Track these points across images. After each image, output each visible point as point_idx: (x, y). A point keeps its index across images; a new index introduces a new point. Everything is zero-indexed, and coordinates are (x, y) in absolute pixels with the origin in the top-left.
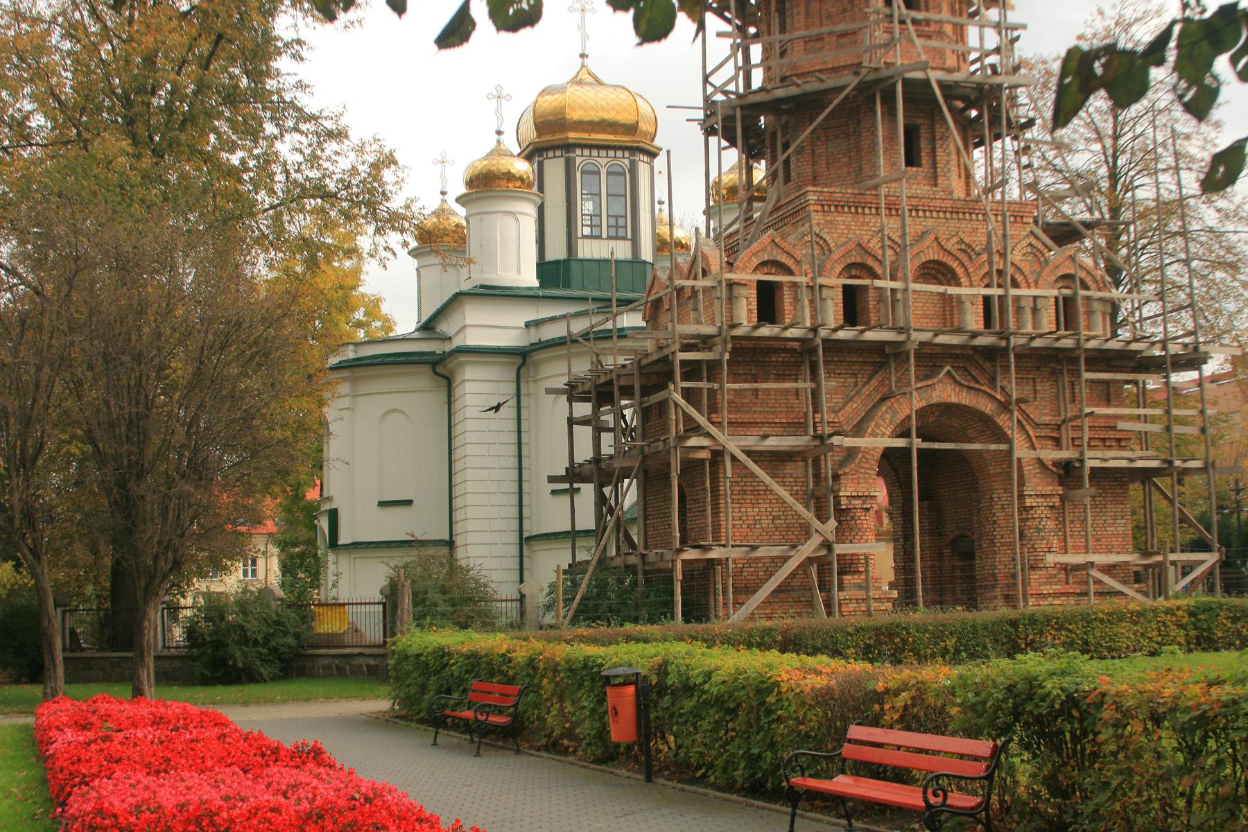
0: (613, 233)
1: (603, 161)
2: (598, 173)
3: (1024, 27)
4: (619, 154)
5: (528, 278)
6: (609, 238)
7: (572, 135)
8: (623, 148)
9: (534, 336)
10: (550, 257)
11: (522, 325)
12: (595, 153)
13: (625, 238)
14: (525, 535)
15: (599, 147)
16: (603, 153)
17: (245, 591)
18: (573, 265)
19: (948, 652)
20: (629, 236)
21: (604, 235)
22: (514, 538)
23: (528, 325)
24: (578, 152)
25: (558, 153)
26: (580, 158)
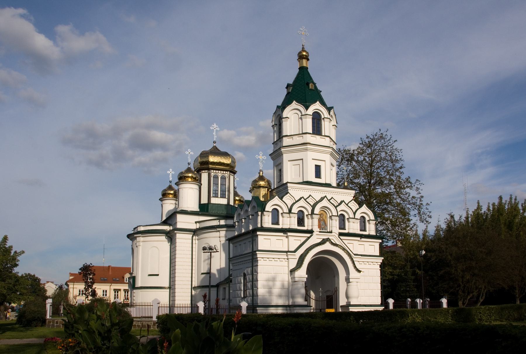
0: (214, 195)
3: (511, 195)
5: (196, 209)
7: (210, 166)
9: (198, 226)
10: (202, 203)
12: (217, 171)
14: (193, 286)
15: (218, 170)
16: (220, 172)
17: (83, 303)
18: (210, 205)
21: (219, 196)
24: (212, 171)
25: (206, 171)
26: (213, 173)
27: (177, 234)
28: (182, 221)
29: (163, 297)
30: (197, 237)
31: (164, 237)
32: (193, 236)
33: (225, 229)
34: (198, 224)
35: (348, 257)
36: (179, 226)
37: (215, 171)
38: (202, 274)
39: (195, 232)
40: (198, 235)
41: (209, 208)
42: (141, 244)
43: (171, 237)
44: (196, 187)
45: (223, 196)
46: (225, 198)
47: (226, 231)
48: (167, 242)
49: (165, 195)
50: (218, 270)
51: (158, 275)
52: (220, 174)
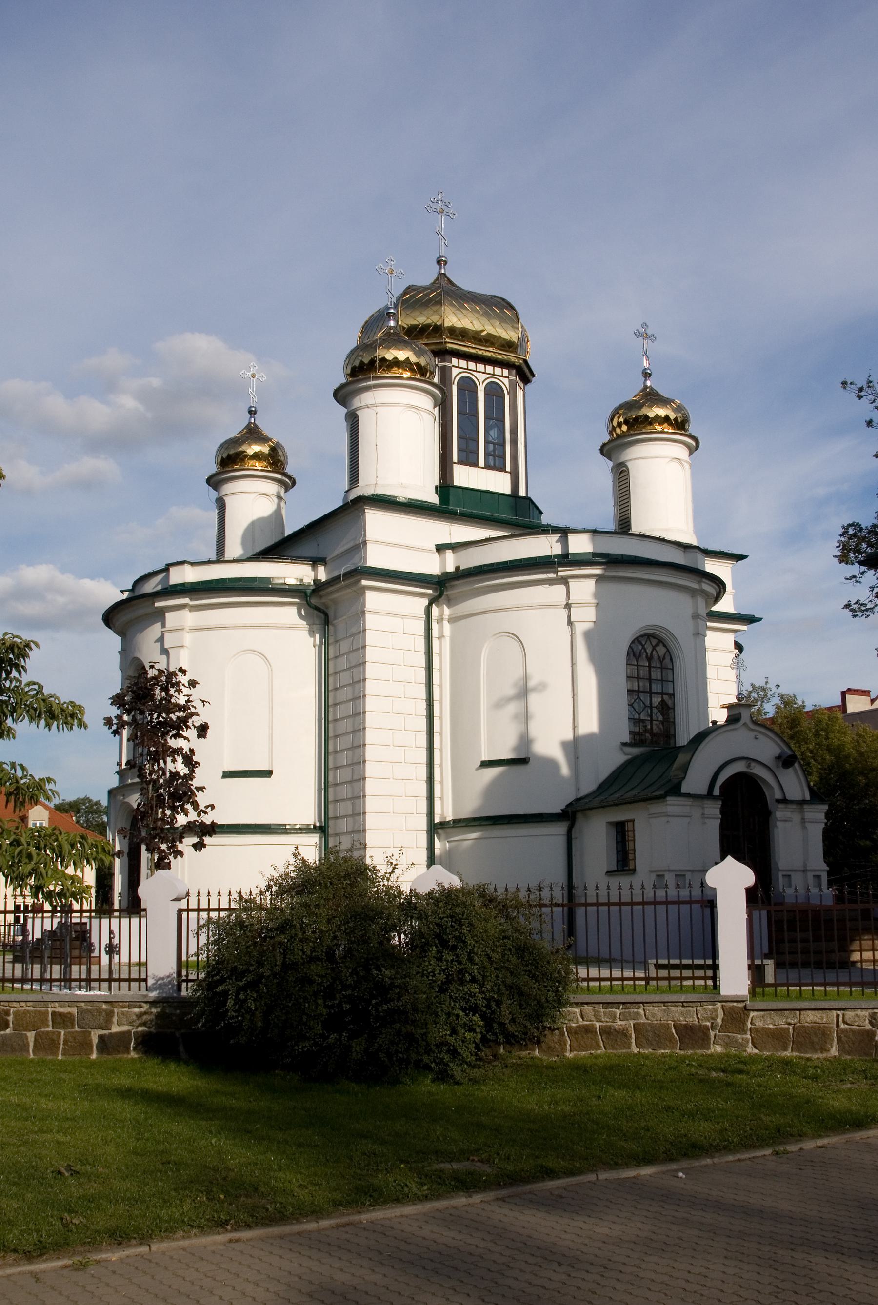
6: (487, 467)
9: (450, 562)
12: (472, 365)
16: (481, 367)
20: (508, 468)
21: (482, 462)
22: (424, 826)
24: (455, 361)
27: (369, 595)
28: (388, 541)
29: (808, 816)
30: (447, 611)
31: (294, 610)
32: (430, 604)
33: (597, 571)
34: (449, 554)
36: (375, 558)
37: (463, 363)
38: (486, 764)
39: (441, 587)
40: (450, 603)
42: (188, 638)
43: (329, 610)
44: (425, 402)
45: (495, 463)
46: (502, 469)
47: (599, 579)
48: (305, 633)
49: (231, 460)
50: (565, 745)
51: (268, 773)
52: (482, 375)
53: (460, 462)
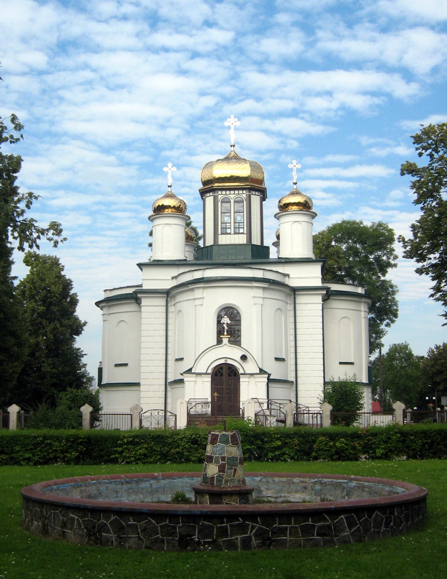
1: (232, 196)
2: (230, 202)
4: (241, 192)
7: (216, 185)
8: (243, 189)
9: (175, 283)
11: (170, 278)
12: (228, 192)
13: (243, 233)
14: (169, 380)
15: (230, 189)
16: (232, 192)
19: (81, 490)
20: (245, 232)
21: (232, 233)
23: (173, 278)
24: (220, 192)
26: (221, 195)
35: (336, 169)
41: (214, 252)
53: (222, 234)
